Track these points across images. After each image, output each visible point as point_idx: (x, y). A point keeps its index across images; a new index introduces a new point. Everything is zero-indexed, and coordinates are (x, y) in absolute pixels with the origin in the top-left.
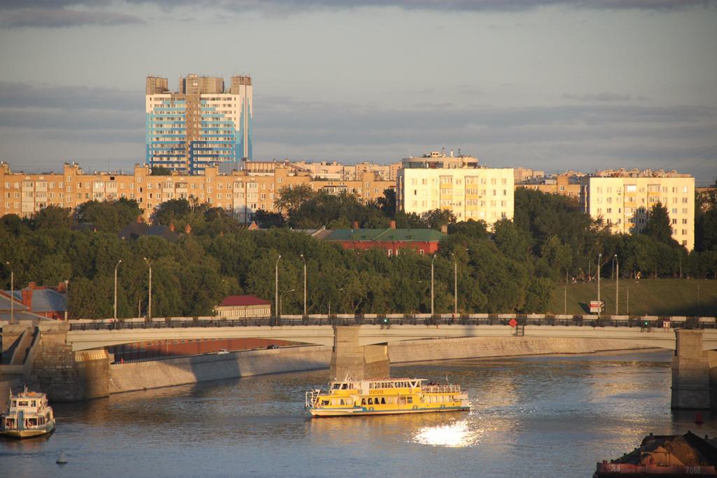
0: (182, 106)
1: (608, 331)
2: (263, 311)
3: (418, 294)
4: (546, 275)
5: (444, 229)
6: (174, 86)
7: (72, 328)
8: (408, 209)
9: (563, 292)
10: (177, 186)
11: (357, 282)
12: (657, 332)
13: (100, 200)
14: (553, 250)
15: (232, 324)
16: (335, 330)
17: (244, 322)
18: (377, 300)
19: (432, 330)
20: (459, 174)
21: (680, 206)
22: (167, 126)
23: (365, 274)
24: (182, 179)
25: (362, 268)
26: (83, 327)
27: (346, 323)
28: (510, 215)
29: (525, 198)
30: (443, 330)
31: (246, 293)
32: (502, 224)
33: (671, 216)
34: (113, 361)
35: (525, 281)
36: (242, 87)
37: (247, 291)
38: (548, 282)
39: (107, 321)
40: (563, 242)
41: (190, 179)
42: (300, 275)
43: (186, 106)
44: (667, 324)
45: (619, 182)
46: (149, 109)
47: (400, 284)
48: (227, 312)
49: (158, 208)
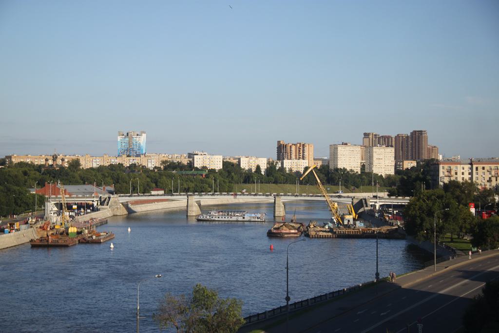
0: (127, 139)
1: (258, 197)
2: (162, 192)
3: (201, 188)
4: (232, 183)
5: (207, 171)
6: (126, 134)
7: (120, 196)
8: (195, 166)
9: (236, 187)
10: (133, 160)
11: (185, 184)
12: (270, 197)
13: (114, 163)
14: (233, 177)
15: (154, 195)
16: (188, 197)
17: (158, 195)
18: (191, 189)
19: (213, 197)
20: (208, 157)
21: (263, 165)
22: (123, 145)
23: (187, 182)
24: (134, 158)
25: (186, 181)
26: (122, 196)
27: (191, 195)
28: (221, 168)
29: (225, 164)
30: (216, 197)
31: (157, 188)
32: (220, 170)
33: (261, 168)
34: (202, 204)
35: (228, 184)
36: (143, 134)
37: (158, 188)
38: (232, 184)
39: (128, 195)
40: (235, 174)
41: (137, 158)
42: (171, 183)
43: (427, 177)
44: (272, 195)
45: (248, 159)
46: (119, 140)
47: (196, 185)
48: (153, 193)
49: (71, 162)
